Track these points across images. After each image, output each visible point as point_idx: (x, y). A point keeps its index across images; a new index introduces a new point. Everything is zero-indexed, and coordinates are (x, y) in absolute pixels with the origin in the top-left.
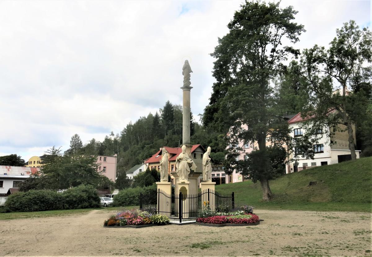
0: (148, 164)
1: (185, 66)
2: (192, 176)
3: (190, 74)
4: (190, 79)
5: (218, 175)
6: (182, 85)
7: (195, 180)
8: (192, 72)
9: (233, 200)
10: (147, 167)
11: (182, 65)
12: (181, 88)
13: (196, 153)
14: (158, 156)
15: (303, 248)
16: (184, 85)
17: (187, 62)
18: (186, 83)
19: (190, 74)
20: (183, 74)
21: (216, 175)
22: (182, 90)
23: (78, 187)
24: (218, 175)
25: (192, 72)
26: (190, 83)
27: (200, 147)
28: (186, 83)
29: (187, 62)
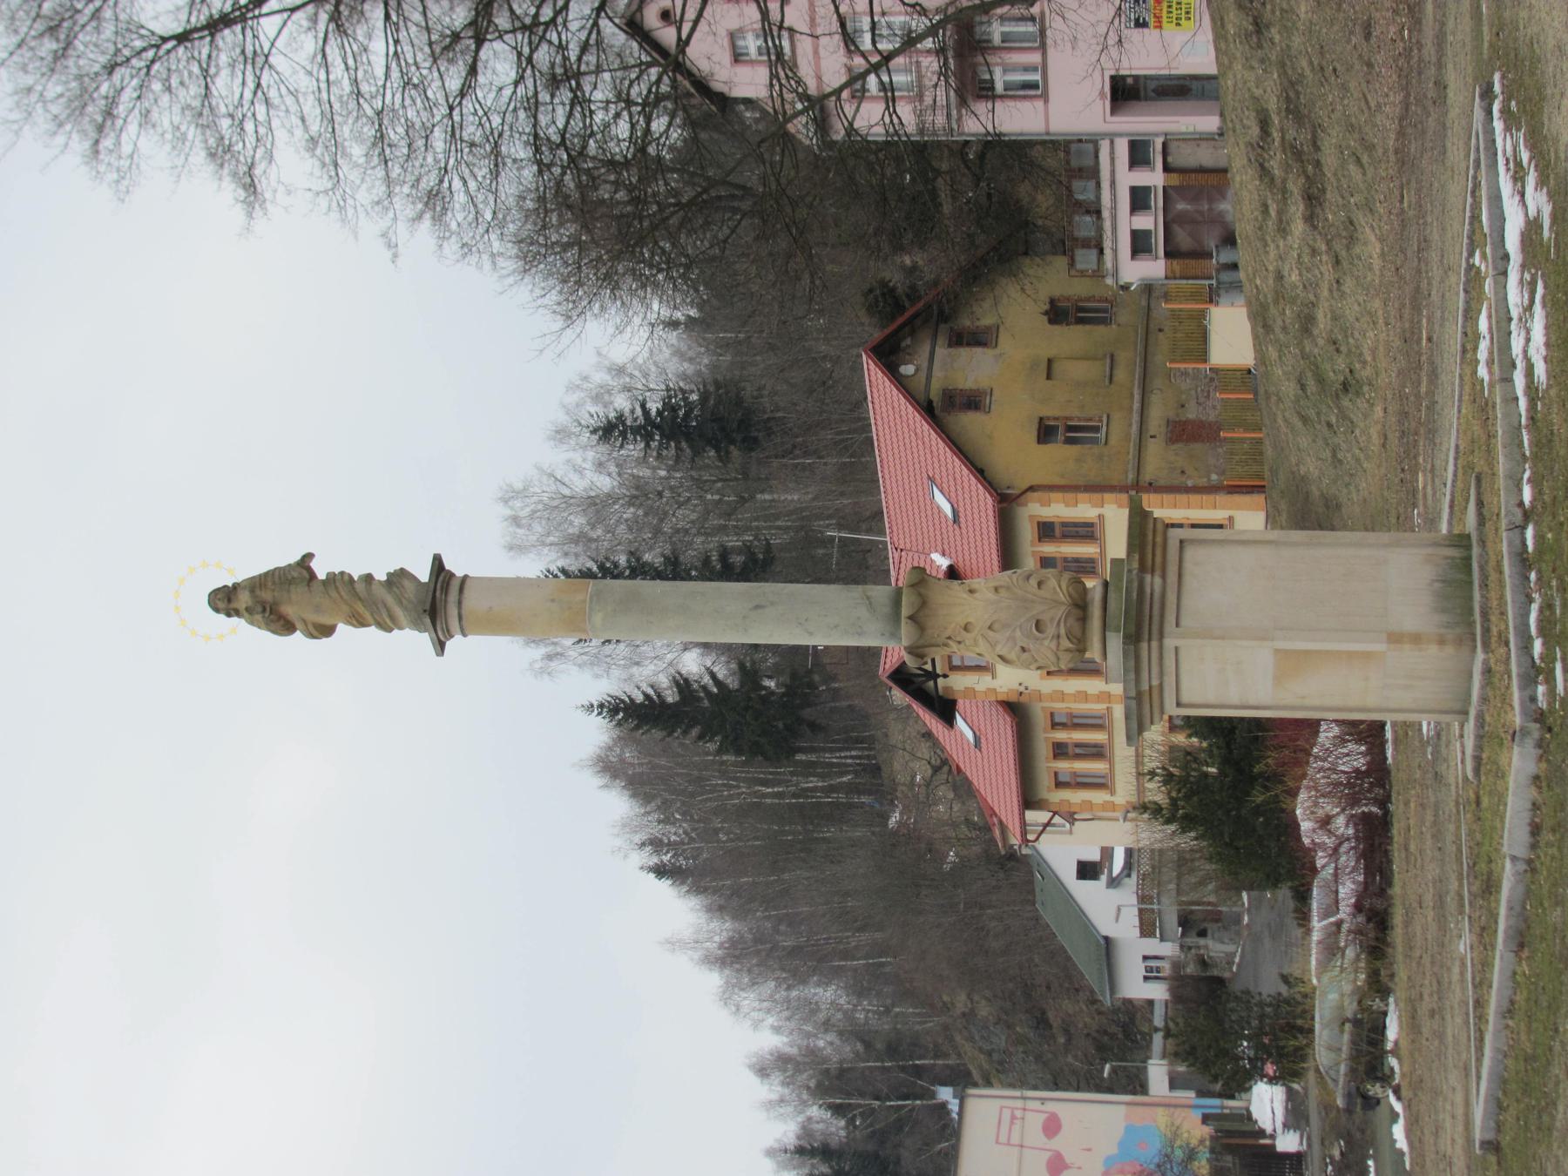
0: (1036, 817)
1: (259, 617)
2: (1158, 580)
3: (321, 576)
4: (369, 578)
5: (1139, 199)
6: (413, 641)
7: (1190, 553)
8: (309, 556)
9: (1176, 1106)
10: (1057, 819)
11: (244, 634)
12: (440, 647)
13: (935, 395)
14: (960, 722)
15: (1463, 346)
16: (417, 625)
17: (224, 600)
18: (399, 613)
19: (321, 576)
20: (326, 631)
21: (1144, 222)
22: (455, 644)
23: (633, 475)
24: (1139, 199)
25: (309, 556)
26: (399, 578)
27: (889, 355)
28: (399, 613)
29: (224, 600)
